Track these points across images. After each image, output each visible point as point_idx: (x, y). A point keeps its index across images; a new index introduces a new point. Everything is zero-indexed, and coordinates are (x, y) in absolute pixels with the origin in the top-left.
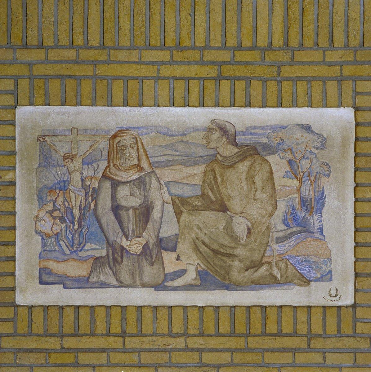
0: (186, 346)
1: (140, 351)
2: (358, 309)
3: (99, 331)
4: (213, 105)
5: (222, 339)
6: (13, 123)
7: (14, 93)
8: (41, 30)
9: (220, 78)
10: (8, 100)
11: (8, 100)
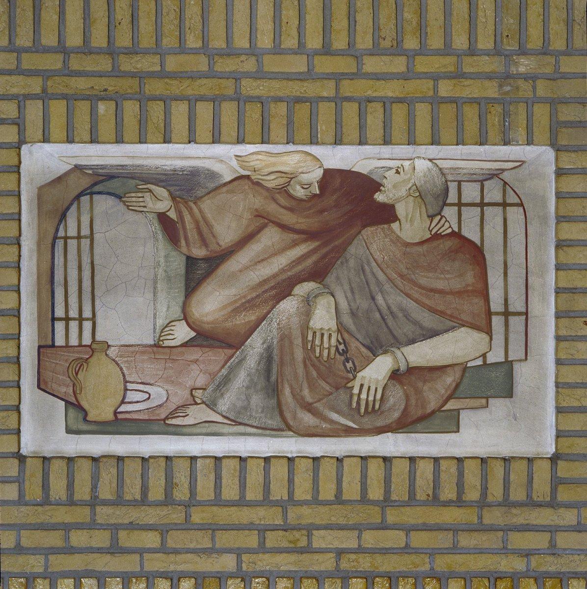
0: (579, 523)
1: (408, 529)
2: (561, 464)
3: (420, 496)
4: (208, 141)
5: (323, 509)
6: (16, 169)
7: (19, 123)
8: (111, 26)
9: (45, 96)
10: (10, 134)
11: (10, 134)
